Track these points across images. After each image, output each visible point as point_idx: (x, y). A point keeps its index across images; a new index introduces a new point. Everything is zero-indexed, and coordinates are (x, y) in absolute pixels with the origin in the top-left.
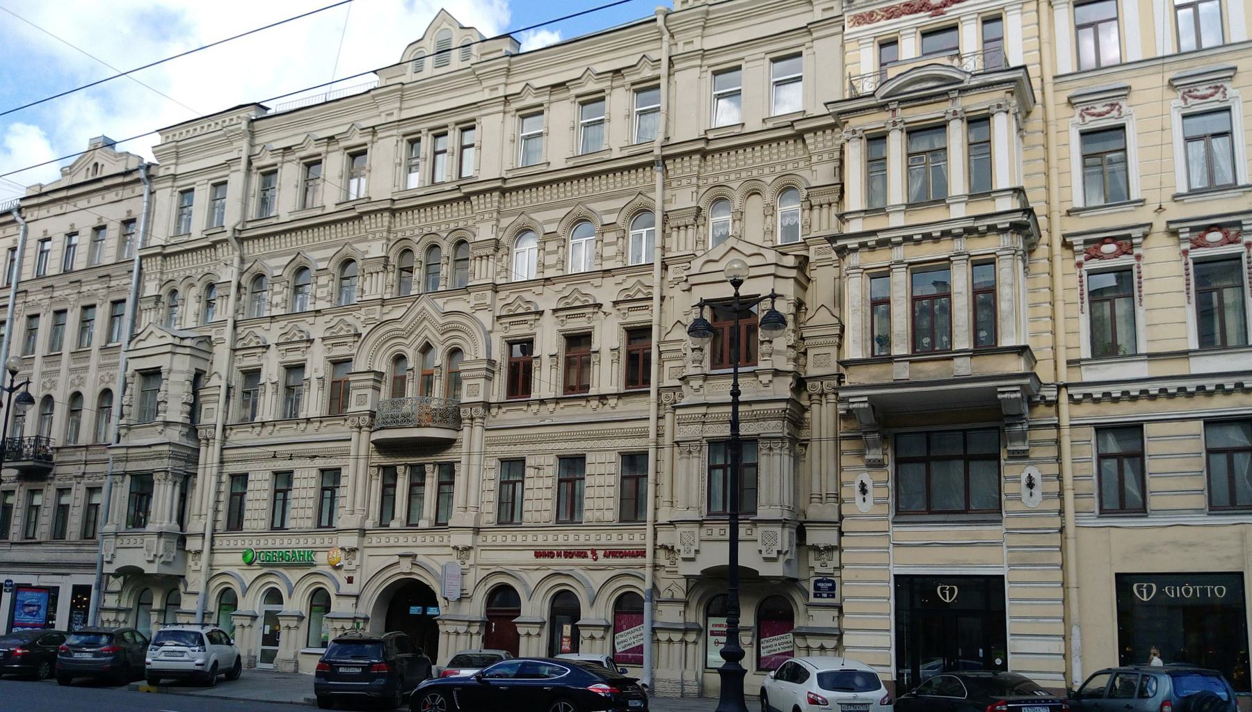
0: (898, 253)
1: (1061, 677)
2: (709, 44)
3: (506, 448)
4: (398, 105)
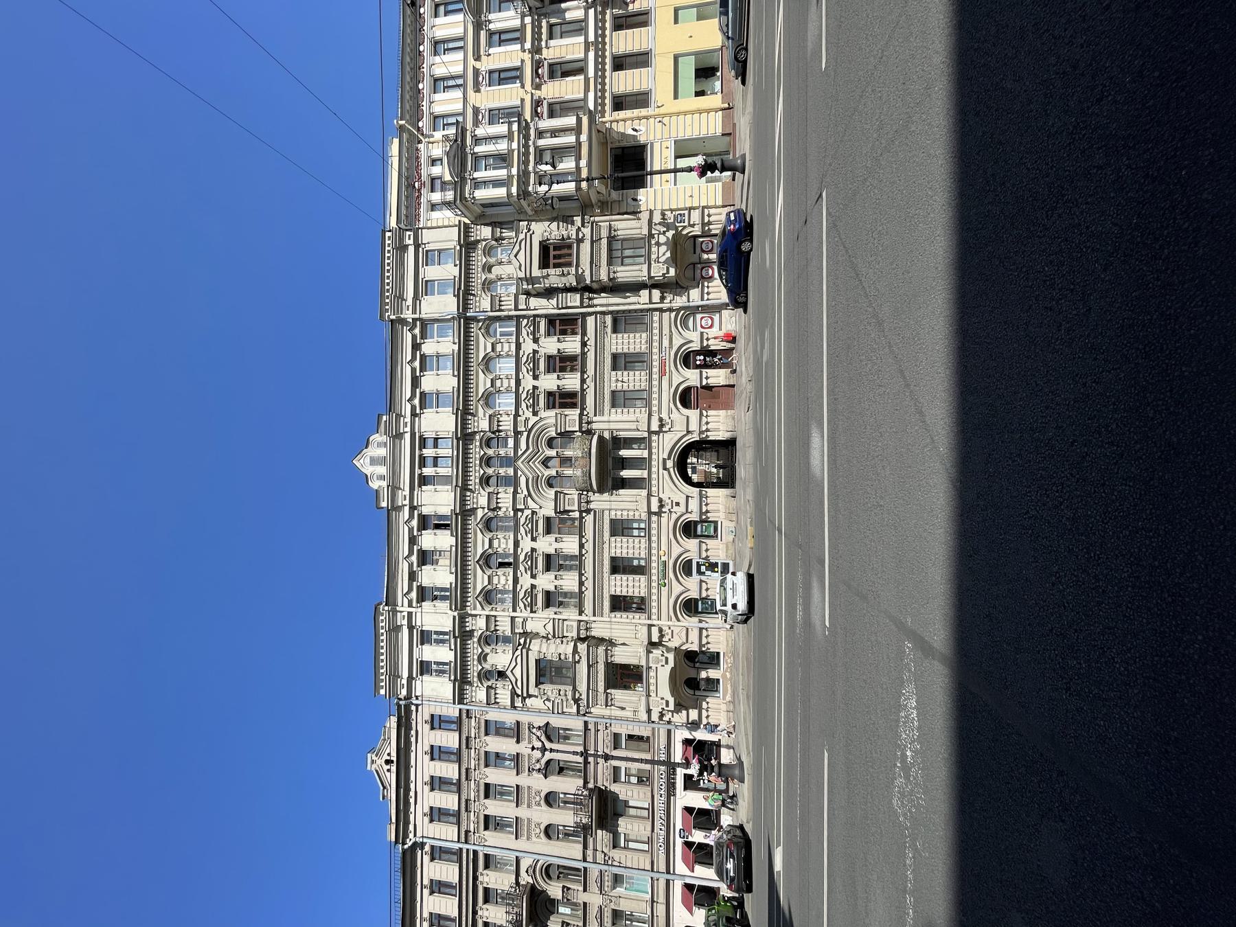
0: (531, 168)
1: (717, 114)
2: (405, 674)
3: (606, 404)
4: (400, 491)
